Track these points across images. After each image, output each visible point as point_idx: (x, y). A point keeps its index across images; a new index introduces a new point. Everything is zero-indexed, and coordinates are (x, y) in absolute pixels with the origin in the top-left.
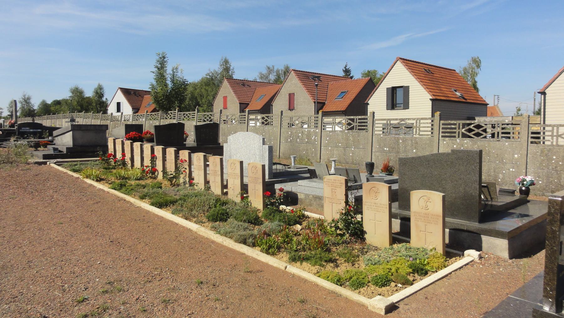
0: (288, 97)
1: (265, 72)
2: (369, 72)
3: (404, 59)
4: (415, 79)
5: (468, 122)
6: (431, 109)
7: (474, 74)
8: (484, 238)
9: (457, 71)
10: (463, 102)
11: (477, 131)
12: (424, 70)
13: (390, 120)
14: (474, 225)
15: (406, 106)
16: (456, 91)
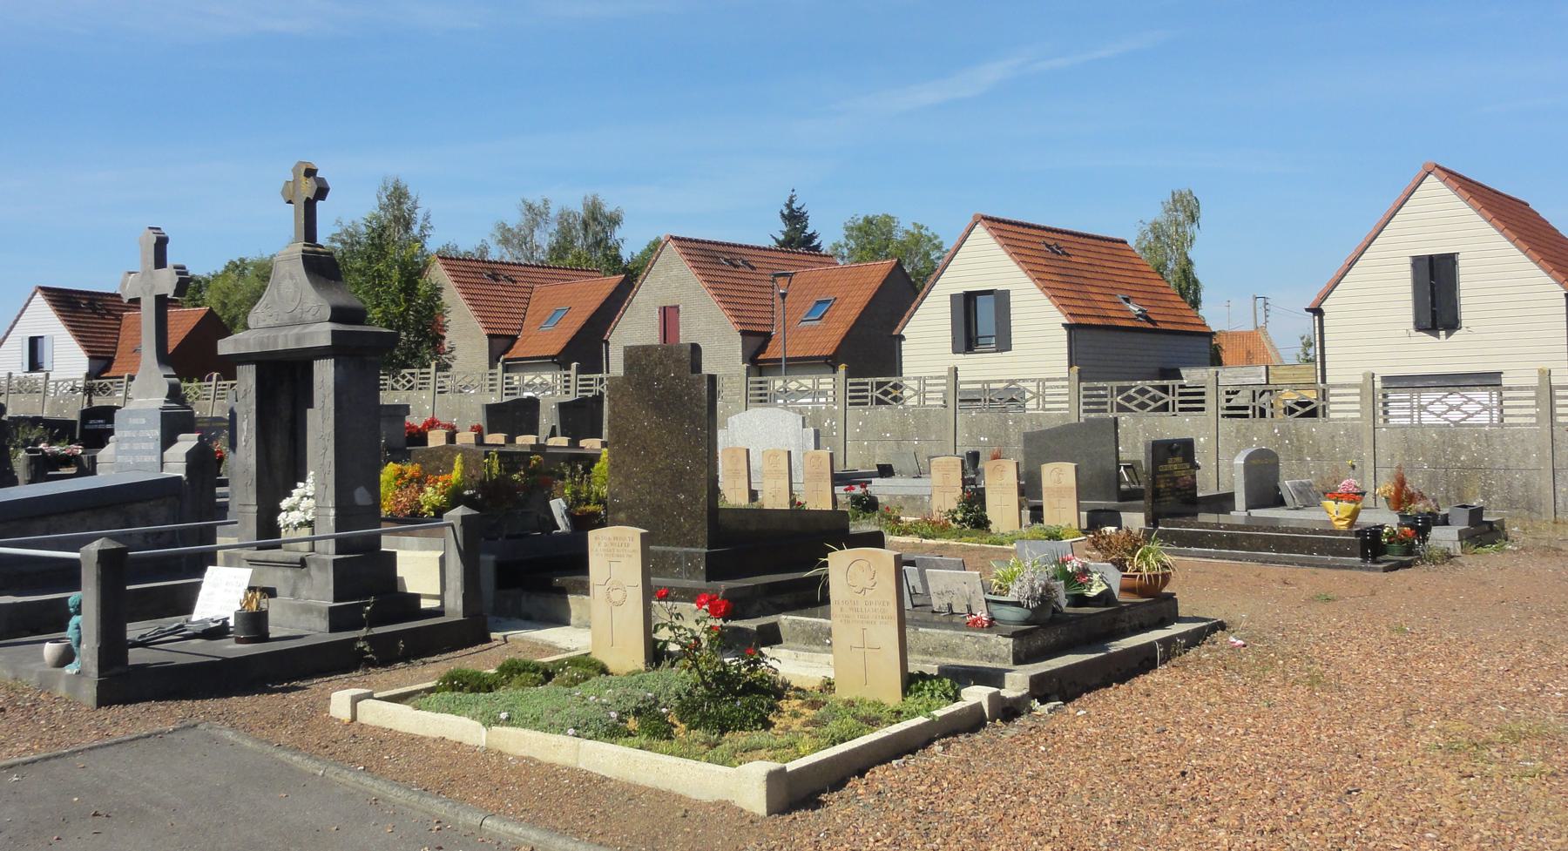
0: (657, 316)
1: (515, 219)
2: (869, 221)
3: (992, 219)
4: (1022, 274)
5: (1126, 384)
6: (1066, 351)
7: (1187, 241)
8: (1123, 514)
9: (1132, 243)
10: (1148, 330)
11: (1140, 399)
12: (1043, 247)
13: (988, 382)
14: (1113, 504)
15: (1004, 344)
16: (1127, 300)
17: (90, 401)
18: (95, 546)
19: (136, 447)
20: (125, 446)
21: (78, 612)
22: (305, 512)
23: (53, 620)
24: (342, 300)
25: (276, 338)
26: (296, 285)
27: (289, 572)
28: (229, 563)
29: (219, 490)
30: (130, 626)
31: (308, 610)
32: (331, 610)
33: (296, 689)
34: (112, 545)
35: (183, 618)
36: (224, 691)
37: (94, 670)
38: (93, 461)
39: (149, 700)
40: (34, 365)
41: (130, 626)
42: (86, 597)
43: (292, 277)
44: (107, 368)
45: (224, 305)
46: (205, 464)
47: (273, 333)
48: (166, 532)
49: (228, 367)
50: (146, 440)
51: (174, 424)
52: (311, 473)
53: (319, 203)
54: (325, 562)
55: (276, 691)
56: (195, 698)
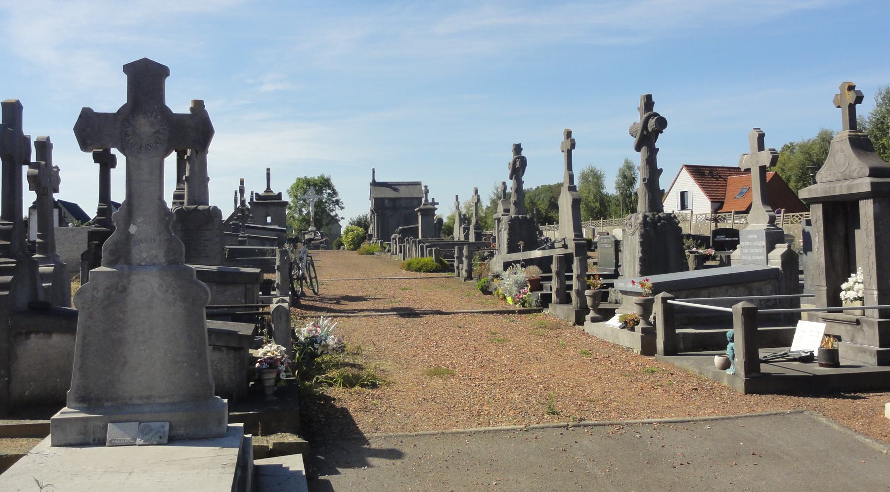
17: (716, 226)
18: (740, 306)
19: (752, 251)
20: (746, 251)
21: (732, 341)
22: (857, 291)
23: (718, 344)
24: (877, 162)
25: (834, 188)
26: (845, 156)
27: (849, 327)
28: (811, 319)
29: (800, 276)
30: (760, 350)
31: (863, 351)
32: (878, 352)
33: (860, 398)
34: (750, 305)
35: (787, 349)
36: (817, 394)
37: (743, 373)
38: (729, 258)
39: (773, 393)
40: (683, 207)
41: (760, 350)
42: (736, 332)
43: (842, 151)
44: (721, 207)
45: (783, 170)
46: (790, 259)
47: (832, 185)
48: (774, 301)
49: (803, 206)
50: (758, 247)
51: (774, 238)
52: (859, 269)
53: (857, 106)
54: (873, 323)
55: (844, 398)
56: (799, 396)
